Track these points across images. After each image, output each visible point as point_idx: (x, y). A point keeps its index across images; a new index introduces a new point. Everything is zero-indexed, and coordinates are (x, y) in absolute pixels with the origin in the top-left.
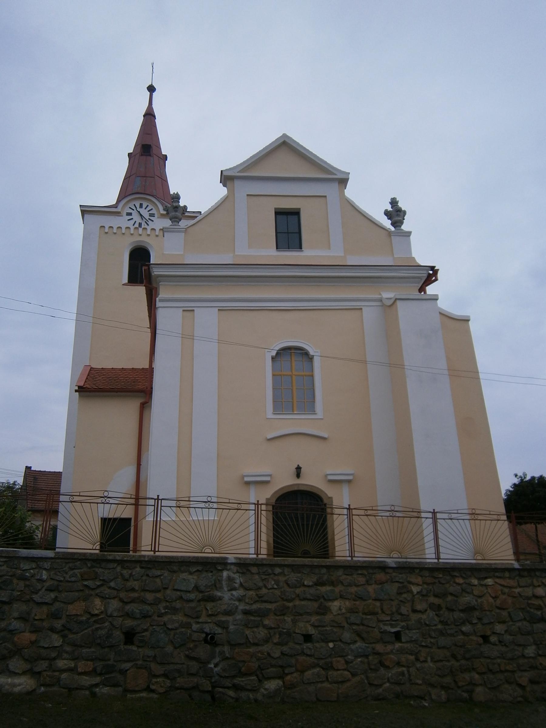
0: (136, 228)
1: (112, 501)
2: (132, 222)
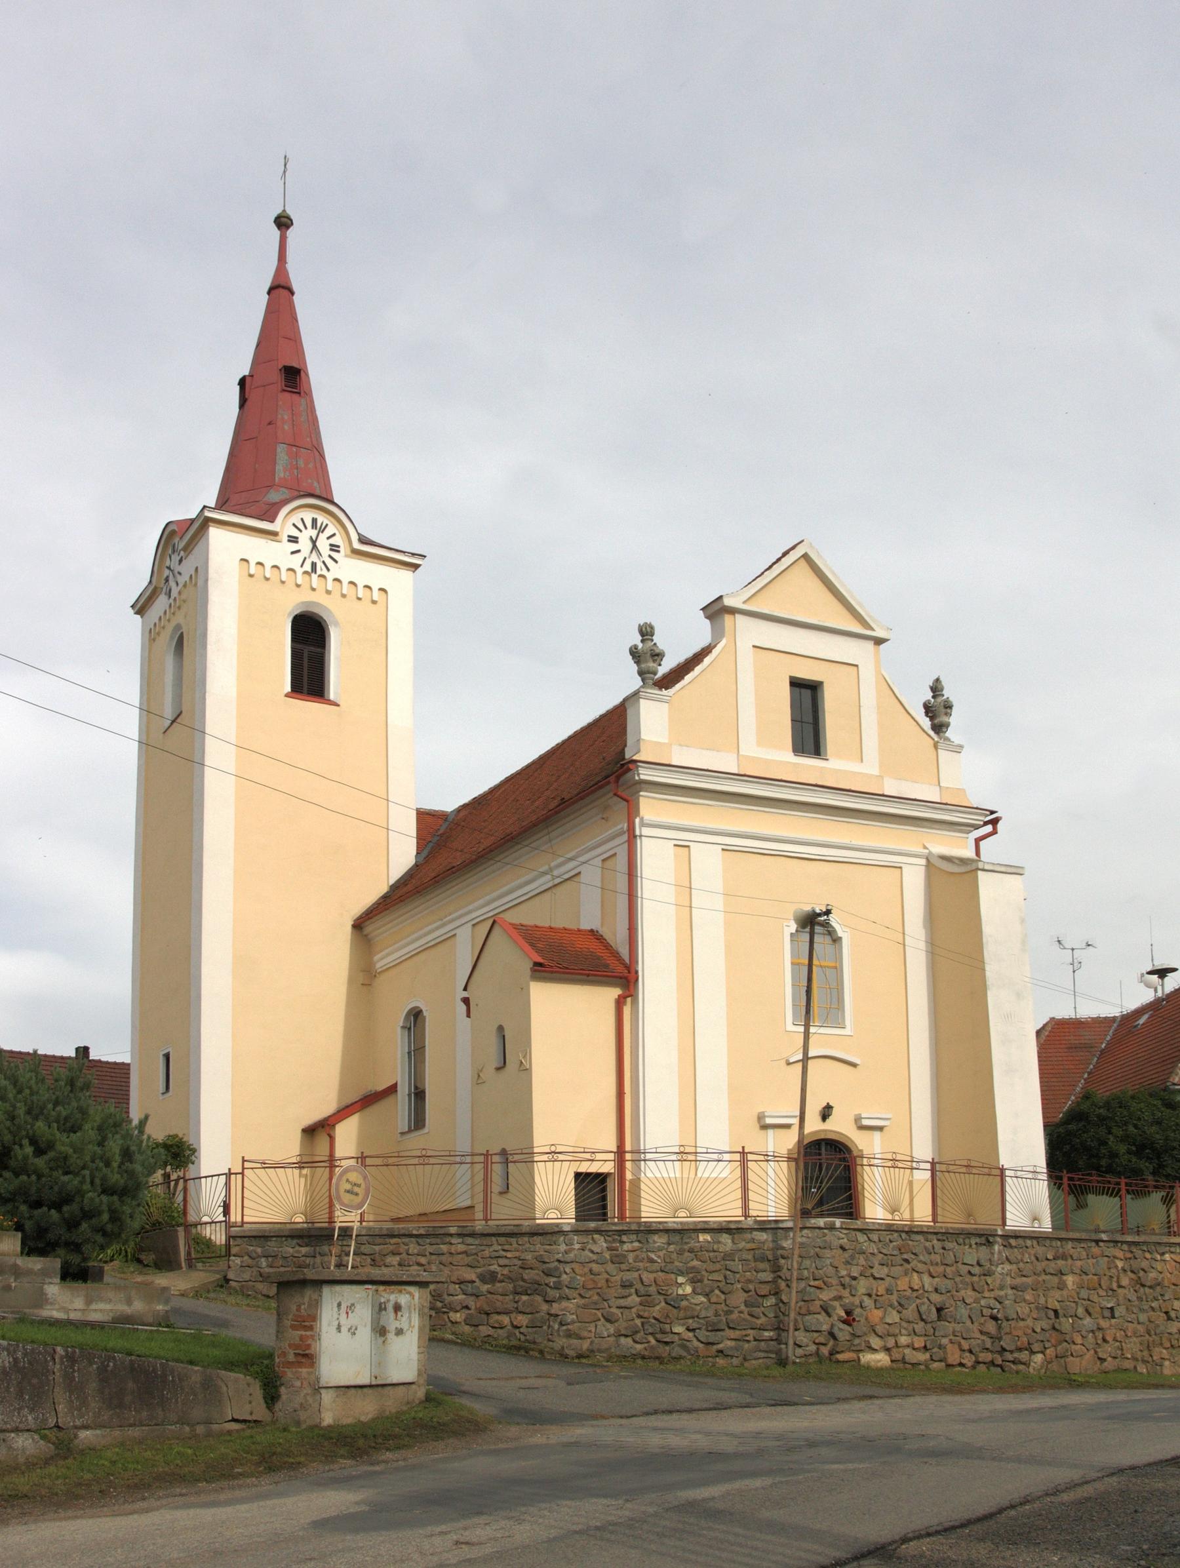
0: (306, 572)
2: (299, 558)
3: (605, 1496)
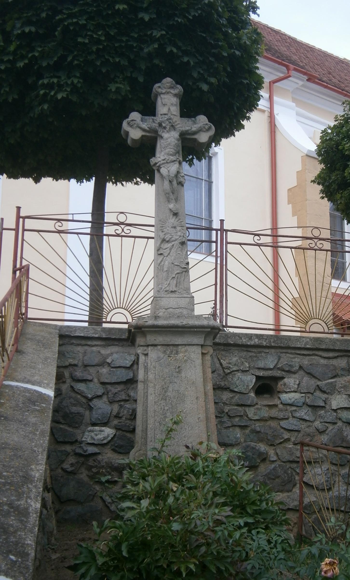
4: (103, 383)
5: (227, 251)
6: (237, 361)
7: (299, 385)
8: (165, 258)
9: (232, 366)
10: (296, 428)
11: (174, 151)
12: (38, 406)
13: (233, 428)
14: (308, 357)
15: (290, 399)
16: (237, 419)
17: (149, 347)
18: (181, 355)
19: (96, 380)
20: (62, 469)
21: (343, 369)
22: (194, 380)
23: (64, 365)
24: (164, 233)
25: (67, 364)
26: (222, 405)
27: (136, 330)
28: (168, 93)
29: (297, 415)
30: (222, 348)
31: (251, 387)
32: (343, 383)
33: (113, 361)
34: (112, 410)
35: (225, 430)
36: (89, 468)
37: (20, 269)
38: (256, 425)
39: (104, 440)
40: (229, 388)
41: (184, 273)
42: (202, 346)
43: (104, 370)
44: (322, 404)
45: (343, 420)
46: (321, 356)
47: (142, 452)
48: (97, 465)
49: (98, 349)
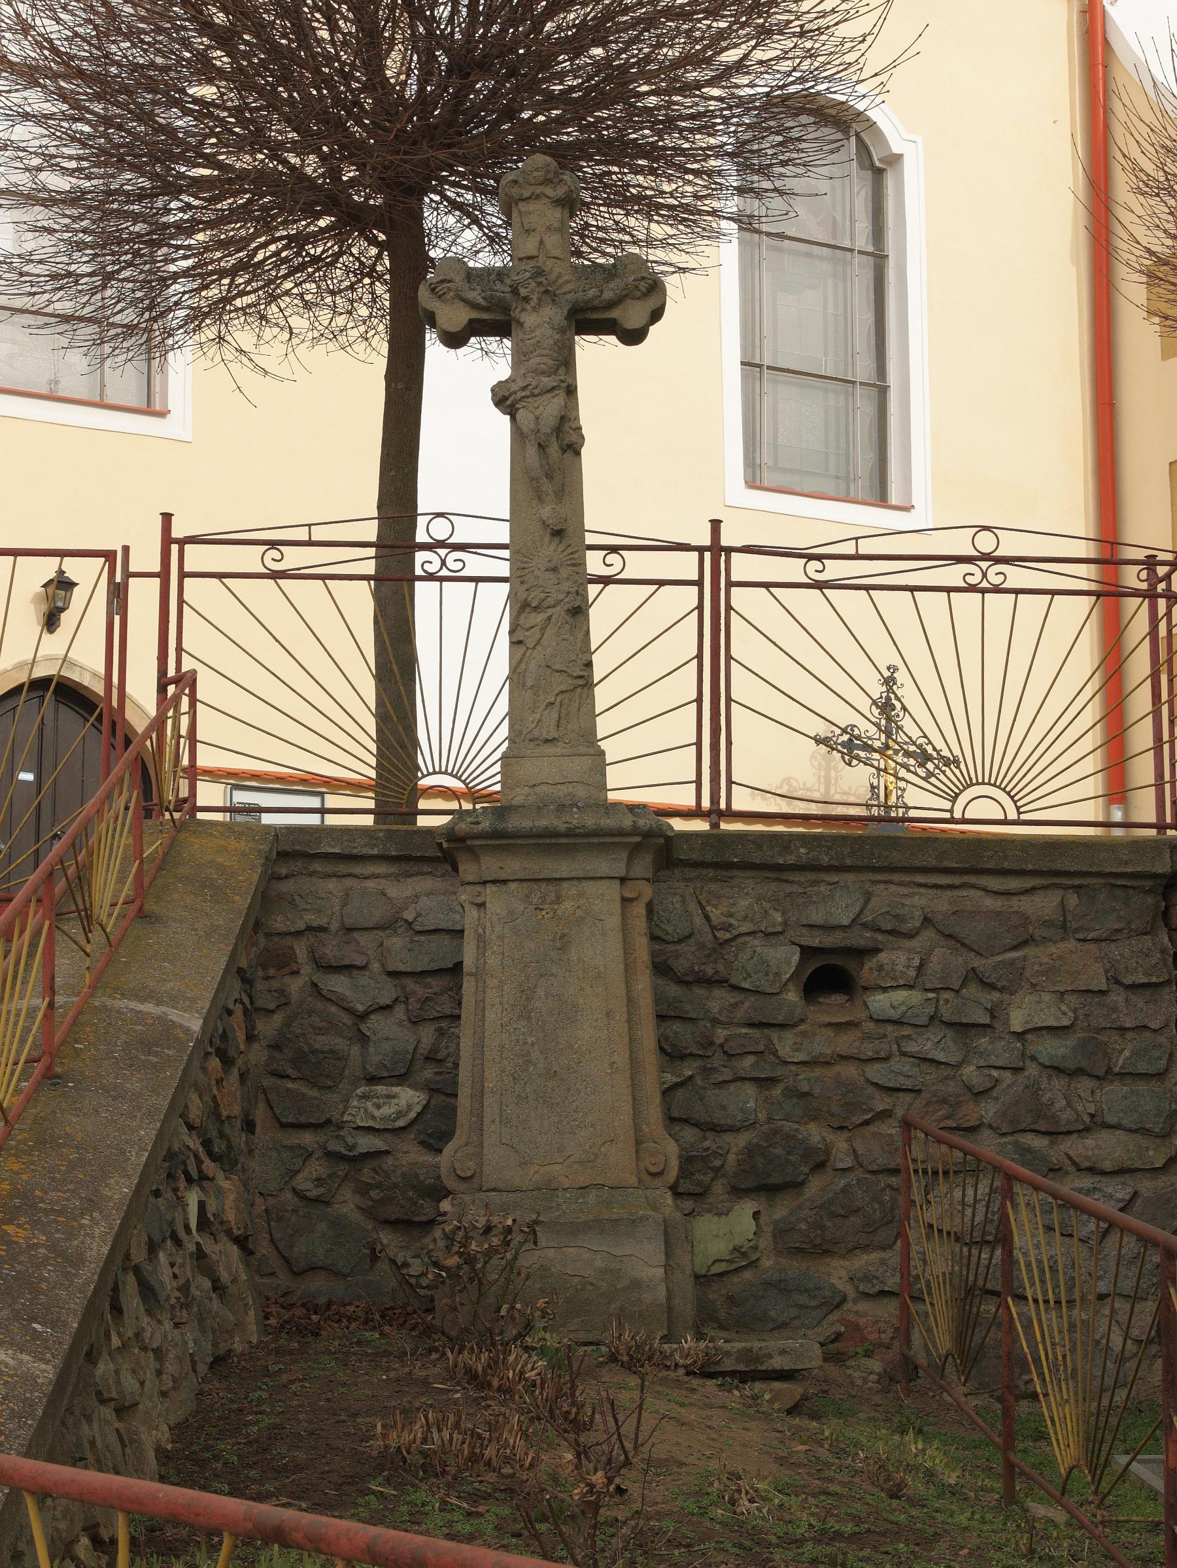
1: (1016, 577)
3: (121, 1226)
4: (394, 974)
5: (729, 608)
6: (750, 907)
7: (920, 968)
8: (528, 654)
9: (735, 923)
10: (908, 1084)
11: (551, 362)
12: (156, 1054)
13: (739, 1084)
14: (949, 893)
15: (893, 1007)
16: (749, 1061)
17: (488, 885)
18: (568, 905)
19: (376, 966)
20: (294, 1190)
21: (1047, 924)
22: (602, 969)
23: (293, 930)
24: (526, 586)
25: (301, 925)
26: (708, 1025)
27: (452, 845)
28: (538, 197)
29: (913, 1048)
30: (711, 873)
31: (788, 976)
32: (1046, 960)
33: (419, 915)
34: (419, 1042)
35: (717, 1091)
36: (363, 1190)
37: (176, 681)
38: (800, 1077)
39: (397, 1119)
40: (726, 981)
41: (579, 690)
42: (623, 880)
43: (397, 942)
44: (984, 1019)
45: (1041, 1061)
46: (985, 890)
47: (471, 1149)
48: (380, 1183)
49: (383, 884)
